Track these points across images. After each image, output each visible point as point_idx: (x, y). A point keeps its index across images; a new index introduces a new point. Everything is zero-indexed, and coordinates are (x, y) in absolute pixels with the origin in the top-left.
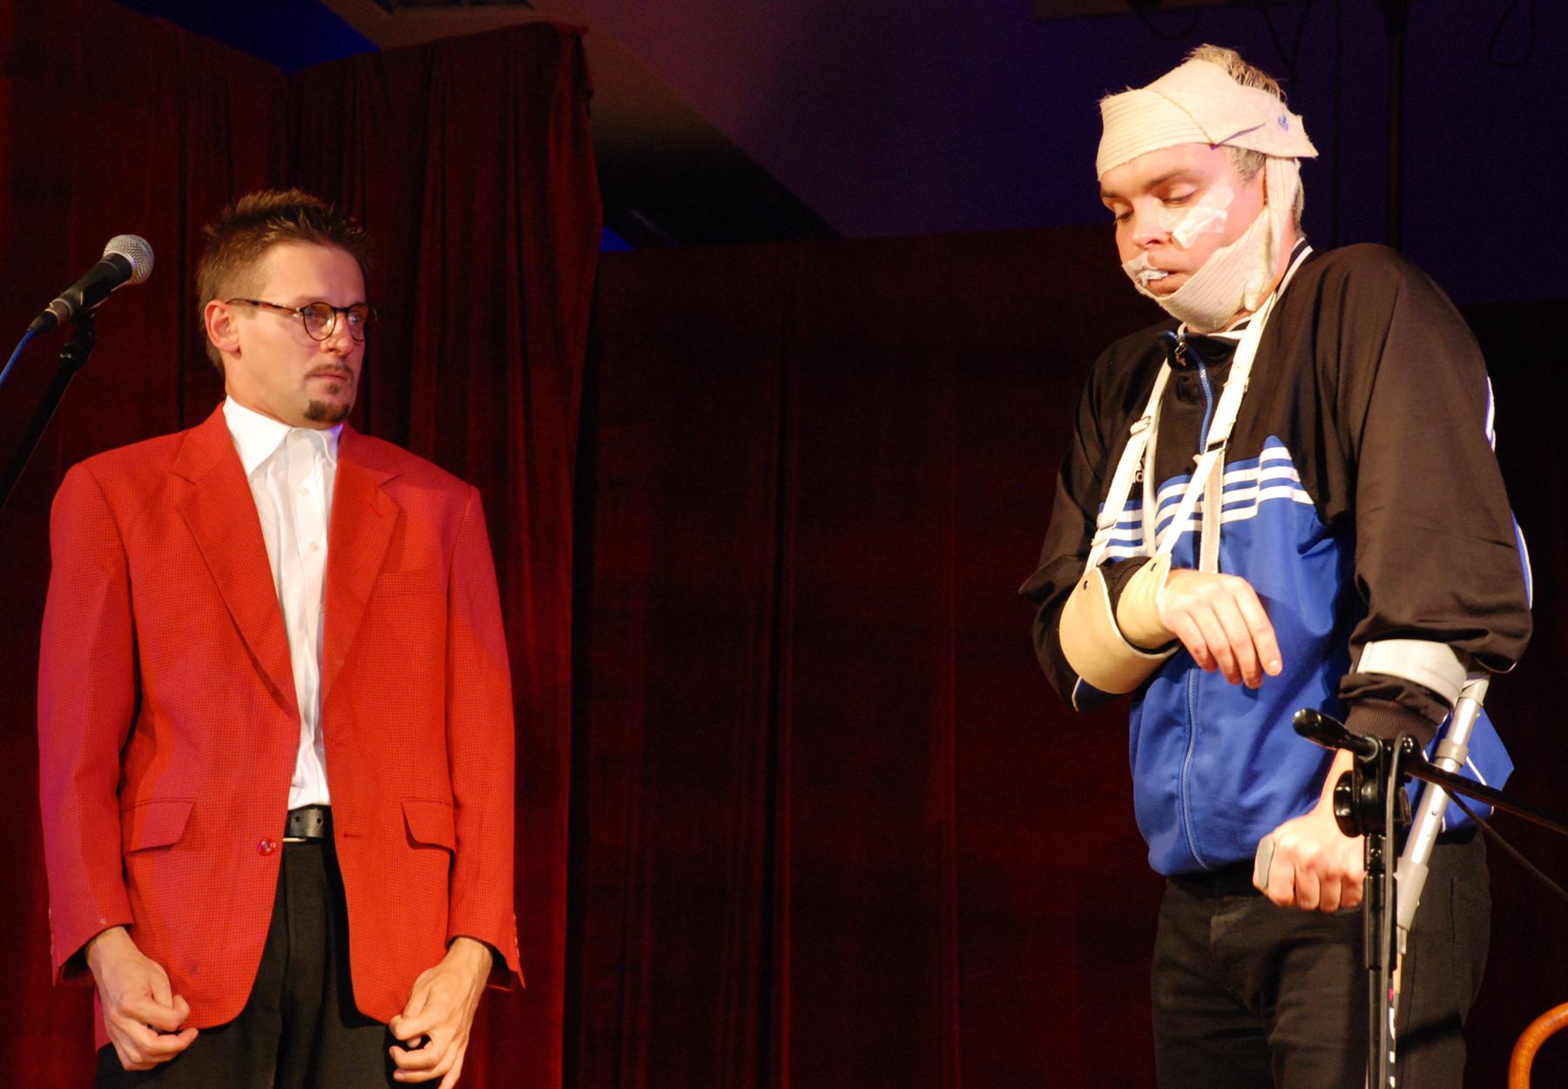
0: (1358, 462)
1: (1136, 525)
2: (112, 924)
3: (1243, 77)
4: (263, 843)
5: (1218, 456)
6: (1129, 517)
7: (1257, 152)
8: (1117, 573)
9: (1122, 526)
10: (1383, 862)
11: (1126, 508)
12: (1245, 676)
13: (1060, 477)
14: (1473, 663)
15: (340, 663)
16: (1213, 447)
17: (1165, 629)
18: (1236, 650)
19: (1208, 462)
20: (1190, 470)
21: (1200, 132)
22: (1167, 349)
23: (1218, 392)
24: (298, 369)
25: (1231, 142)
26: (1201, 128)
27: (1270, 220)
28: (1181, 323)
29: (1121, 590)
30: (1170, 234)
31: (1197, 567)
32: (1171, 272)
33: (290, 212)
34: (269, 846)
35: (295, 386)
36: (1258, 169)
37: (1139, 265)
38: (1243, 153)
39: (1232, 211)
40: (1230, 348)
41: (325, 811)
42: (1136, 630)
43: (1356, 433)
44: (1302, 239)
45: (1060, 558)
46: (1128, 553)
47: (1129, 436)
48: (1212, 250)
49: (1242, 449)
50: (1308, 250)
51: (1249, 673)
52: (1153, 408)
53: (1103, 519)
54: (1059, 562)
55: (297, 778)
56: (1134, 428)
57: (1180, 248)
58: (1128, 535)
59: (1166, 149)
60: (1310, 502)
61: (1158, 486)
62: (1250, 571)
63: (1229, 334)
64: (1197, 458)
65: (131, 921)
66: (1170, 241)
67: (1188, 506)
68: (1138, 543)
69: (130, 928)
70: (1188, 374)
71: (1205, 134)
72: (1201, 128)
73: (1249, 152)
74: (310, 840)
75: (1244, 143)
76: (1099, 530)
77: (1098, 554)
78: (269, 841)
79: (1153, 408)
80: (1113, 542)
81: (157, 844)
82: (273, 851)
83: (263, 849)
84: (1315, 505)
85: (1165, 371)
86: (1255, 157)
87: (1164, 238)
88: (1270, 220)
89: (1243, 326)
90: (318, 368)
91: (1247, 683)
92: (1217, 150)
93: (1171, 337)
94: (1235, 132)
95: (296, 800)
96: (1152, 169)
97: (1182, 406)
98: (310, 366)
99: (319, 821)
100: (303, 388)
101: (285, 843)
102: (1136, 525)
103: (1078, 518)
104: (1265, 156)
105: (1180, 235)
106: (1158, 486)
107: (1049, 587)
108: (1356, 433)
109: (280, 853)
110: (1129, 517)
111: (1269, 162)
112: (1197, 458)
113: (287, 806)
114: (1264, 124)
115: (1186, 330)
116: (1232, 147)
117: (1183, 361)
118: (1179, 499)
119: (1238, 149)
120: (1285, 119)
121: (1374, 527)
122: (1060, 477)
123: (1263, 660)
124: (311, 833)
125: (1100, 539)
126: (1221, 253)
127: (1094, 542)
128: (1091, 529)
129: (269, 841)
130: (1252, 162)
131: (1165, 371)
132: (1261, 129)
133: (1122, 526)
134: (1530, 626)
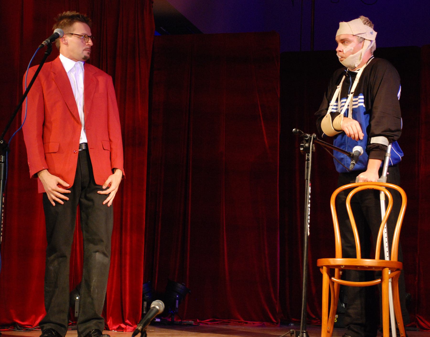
0: (374, 101)
1: (337, 106)
2: (45, 168)
3: (365, 23)
4: (75, 151)
5: (352, 95)
6: (335, 104)
7: (363, 38)
8: (334, 115)
9: (334, 106)
10: (387, 177)
11: (335, 102)
12: (356, 139)
13: (325, 93)
14: (391, 141)
15: (88, 112)
16: (352, 93)
17: (341, 129)
18: (355, 134)
19: (350, 96)
20: (347, 98)
21: (352, 32)
22: (344, 73)
23: (353, 82)
24: (81, 49)
25: (357, 35)
26: (352, 31)
27: (362, 51)
28: (347, 68)
29: (334, 119)
30: (343, 50)
31: (347, 117)
32: (342, 57)
33: (78, 16)
34: (76, 152)
35: (81, 52)
36: (362, 41)
37: (339, 55)
38: (359, 38)
39: (354, 48)
40: (356, 74)
41: (86, 144)
42: (337, 128)
43: (374, 95)
44: (373, 56)
45: (322, 110)
46: (335, 111)
47: (337, 88)
48: (350, 55)
49: (356, 95)
50: (374, 58)
51: (357, 139)
52: (341, 84)
53: (331, 104)
54: (322, 110)
55: (81, 137)
56: (338, 87)
57: (344, 53)
58: (335, 107)
59: (345, 34)
60: (364, 106)
61: (341, 99)
62: (358, 118)
63: (356, 71)
64: (348, 95)
65: (48, 168)
66: (343, 51)
67: (346, 105)
68: (336, 109)
69: (47, 169)
70: (348, 78)
71: (353, 33)
72: (352, 31)
73: (361, 38)
74: (84, 150)
75: (360, 36)
76: (330, 106)
77: (330, 110)
78: (76, 151)
79: (341, 84)
80: (333, 109)
81: (110, 155)
82: (77, 153)
83: (75, 152)
84: (366, 107)
85: (344, 77)
86: (362, 39)
87: (341, 50)
88: (362, 51)
89: (359, 70)
90: (86, 49)
91: (356, 140)
92: (354, 36)
93: (345, 71)
94: (358, 33)
95: (81, 142)
96: (342, 37)
97: (346, 84)
98: (84, 48)
99: (85, 146)
100: (83, 53)
101: (79, 151)
102: (337, 106)
103: (327, 102)
104: (365, 39)
105: (344, 51)
106: (341, 99)
107: (319, 115)
108: (374, 95)
109: (78, 153)
110: (335, 104)
111: (365, 41)
112: (348, 95)
113: (79, 142)
114: (365, 33)
115: (349, 70)
116: (358, 36)
117: (347, 76)
118: (345, 102)
119: (359, 37)
120: (372, 32)
121: (377, 113)
122: (325, 93)
123: (360, 136)
124: (84, 148)
125: (330, 108)
126: (352, 56)
127: (329, 108)
128: (329, 106)
129: (76, 151)
130: (361, 40)
131: (344, 77)
132: (365, 34)
133: (334, 106)
134: (400, 136)
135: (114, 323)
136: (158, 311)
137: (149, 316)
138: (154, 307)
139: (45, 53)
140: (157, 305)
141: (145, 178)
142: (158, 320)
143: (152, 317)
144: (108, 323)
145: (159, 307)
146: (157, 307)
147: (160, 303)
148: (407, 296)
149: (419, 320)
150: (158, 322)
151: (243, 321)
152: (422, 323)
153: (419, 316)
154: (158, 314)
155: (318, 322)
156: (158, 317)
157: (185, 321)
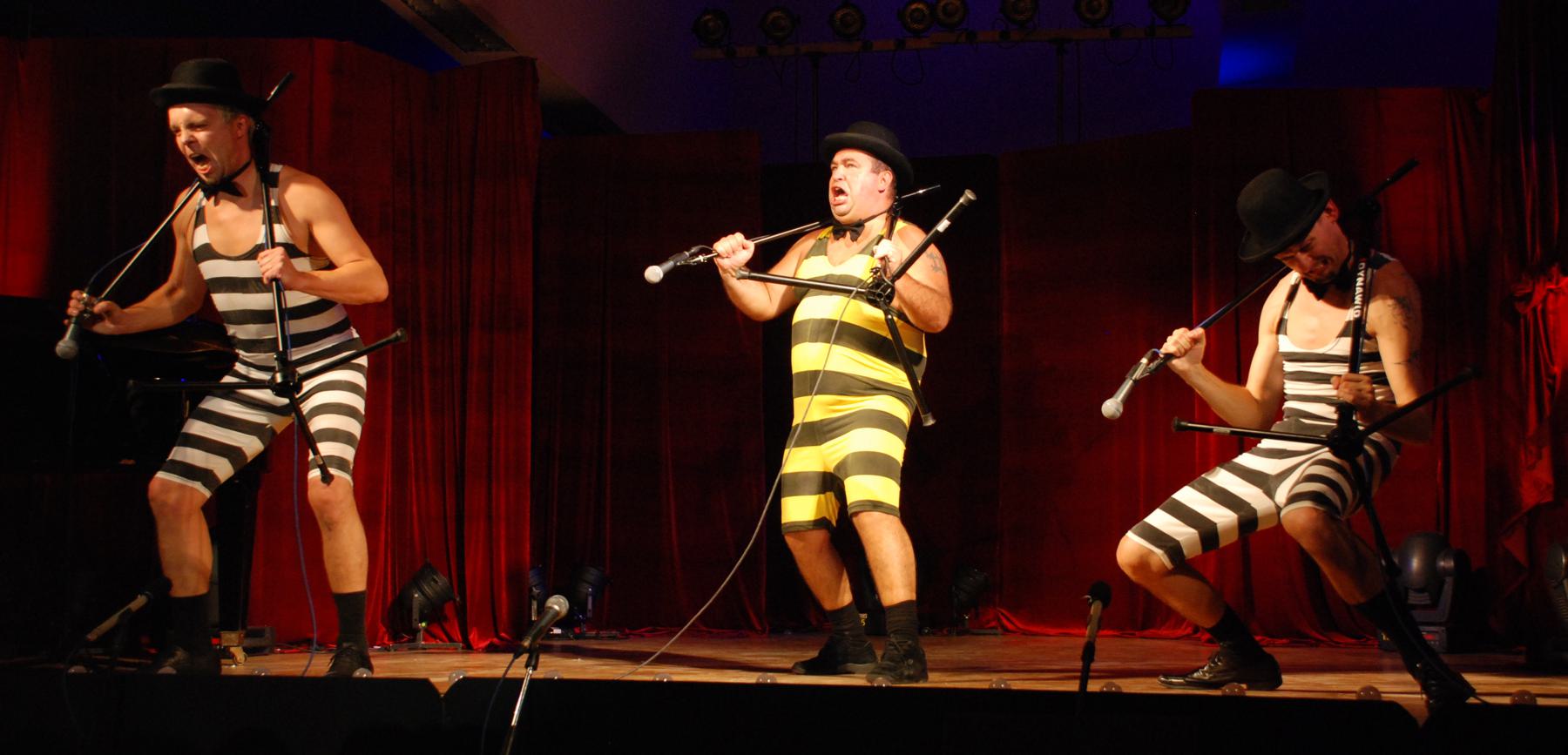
66: (845, 179)
87: (842, 178)
135: (482, 637)
136: (558, 613)
137: (543, 623)
138: (551, 608)
139: (654, 273)
140: (556, 604)
141: (529, 432)
142: (557, 631)
143: (547, 625)
144: (471, 637)
145: (559, 607)
146: (556, 607)
147: (562, 600)
148: (91, 671)
149: (1002, 617)
150: (557, 635)
151: (705, 629)
152: (1005, 622)
153: (1003, 611)
154: (558, 618)
155: (1314, 642)
156: (557, 625)
157: (206, 343)
